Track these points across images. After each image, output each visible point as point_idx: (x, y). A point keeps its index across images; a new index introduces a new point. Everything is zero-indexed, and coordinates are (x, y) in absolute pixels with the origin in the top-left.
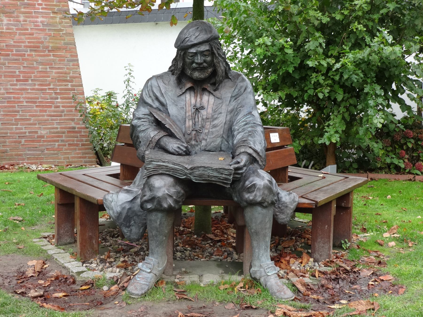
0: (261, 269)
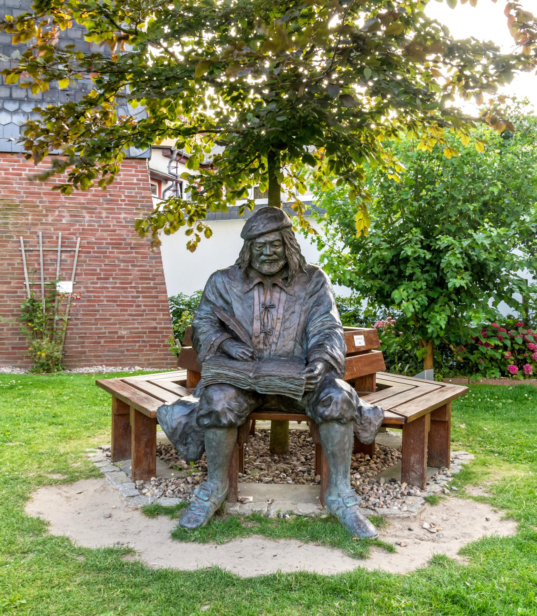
0: (339, 499)
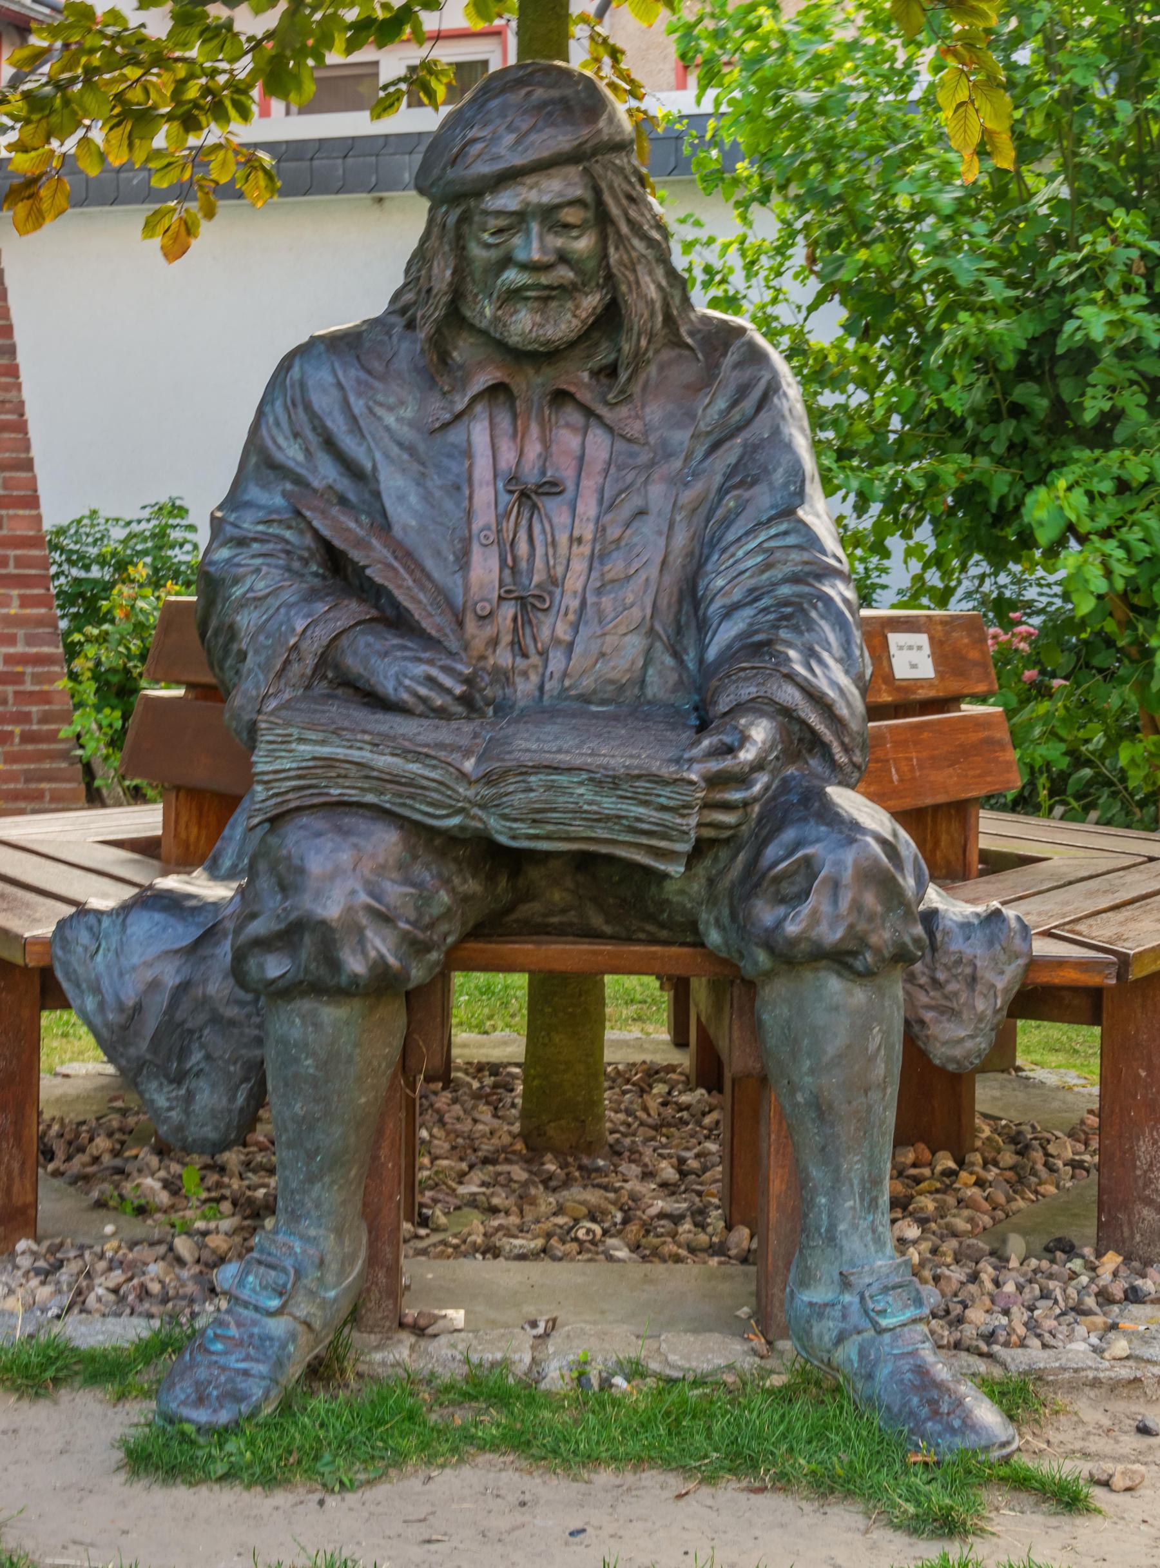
0: (847, 1298)
